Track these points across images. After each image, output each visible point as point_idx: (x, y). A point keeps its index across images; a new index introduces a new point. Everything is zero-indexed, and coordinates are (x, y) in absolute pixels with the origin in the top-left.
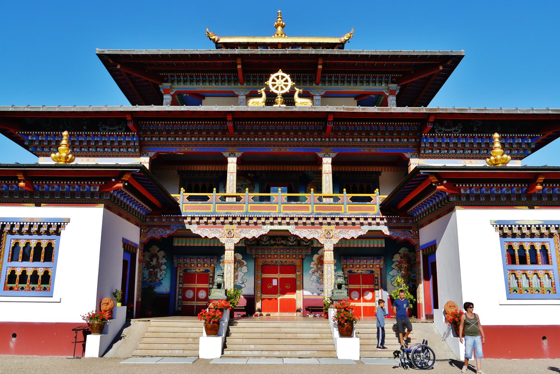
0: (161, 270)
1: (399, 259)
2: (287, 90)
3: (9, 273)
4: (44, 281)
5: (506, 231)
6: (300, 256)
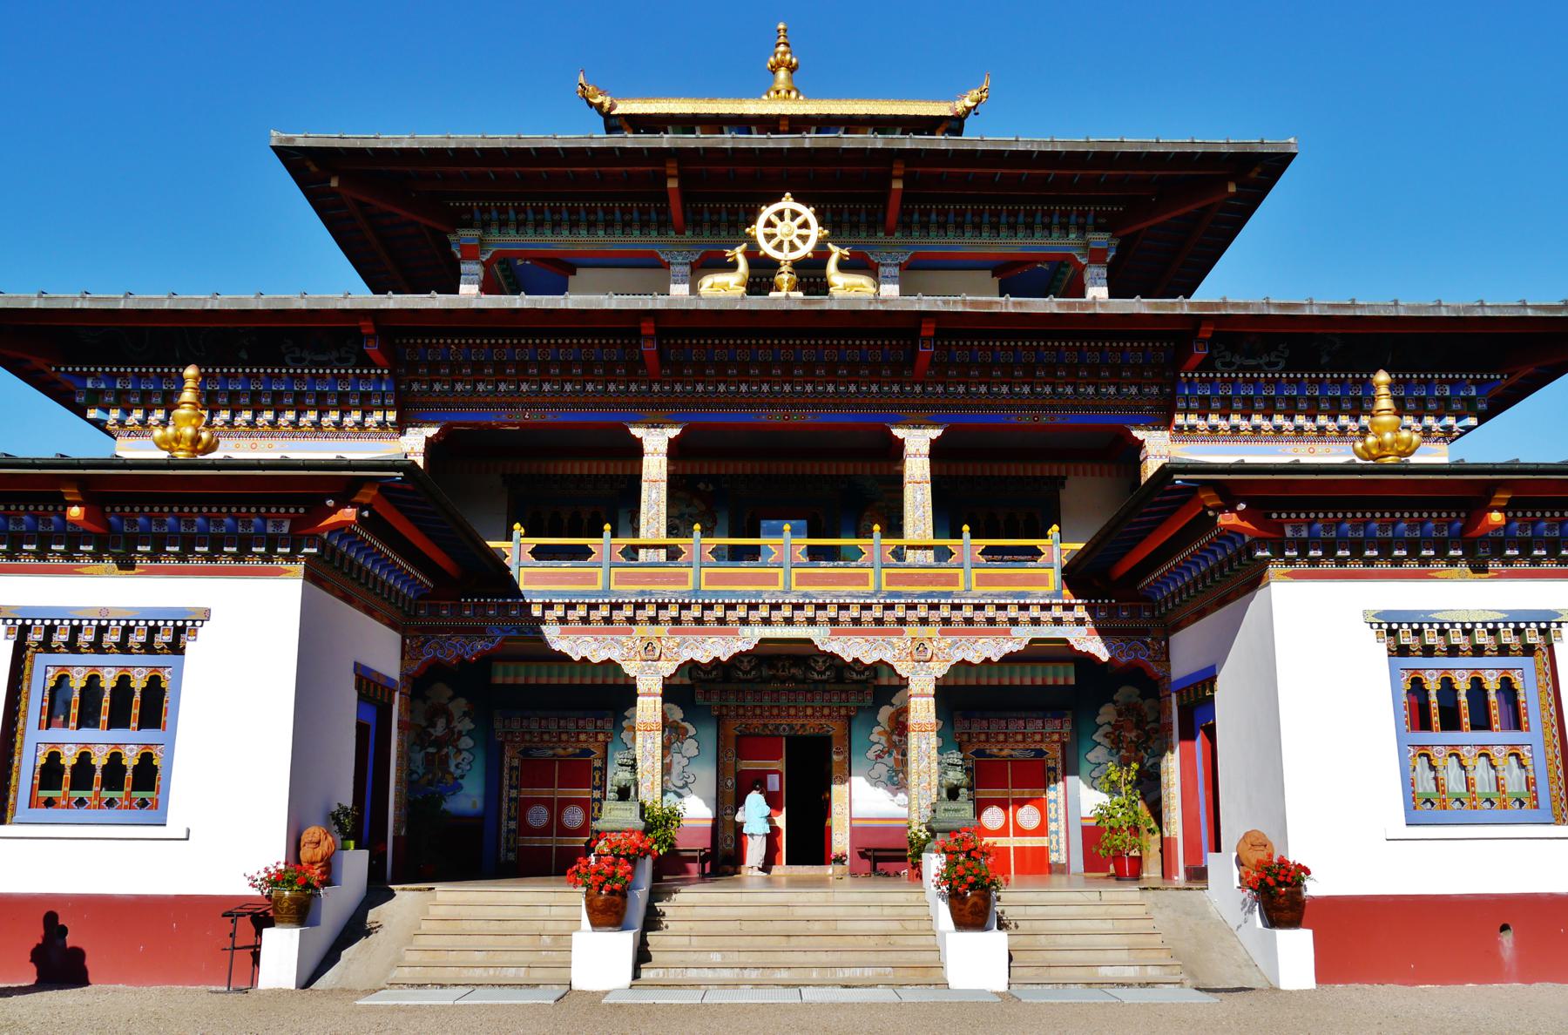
0: (459, 751)
2: (805, 250)
5: (1407, 639)
6: (843, 712)
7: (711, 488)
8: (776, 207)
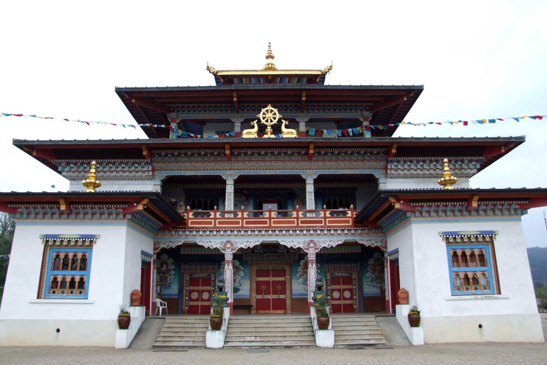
0: (170, 275)
1: (373, 263)
2: (275, 122)
3: (52, 280)
4: (79, 287)
5: (451, 240)
6: (289, 262)
7: (248, 192)
8: (266, 109)
